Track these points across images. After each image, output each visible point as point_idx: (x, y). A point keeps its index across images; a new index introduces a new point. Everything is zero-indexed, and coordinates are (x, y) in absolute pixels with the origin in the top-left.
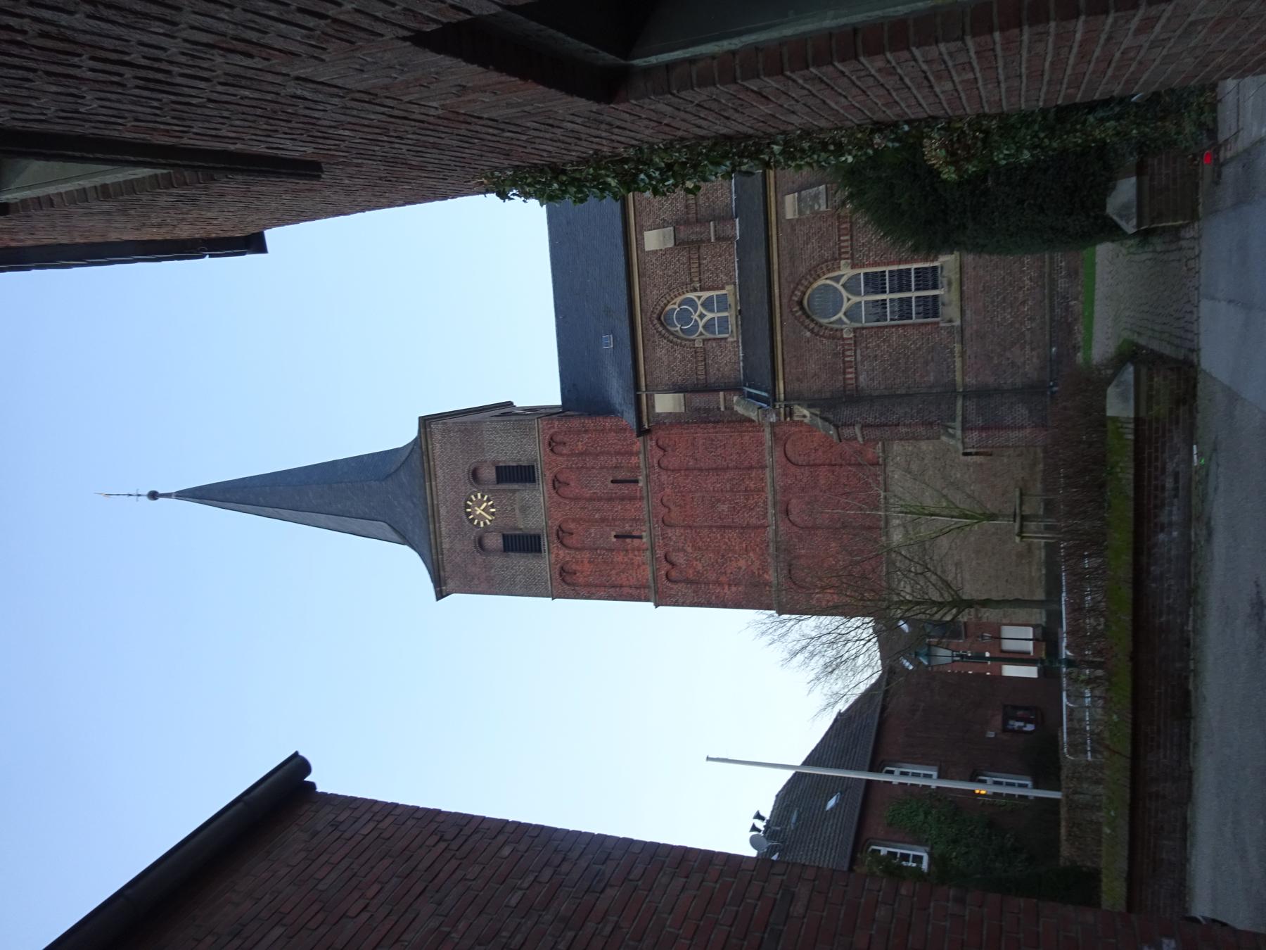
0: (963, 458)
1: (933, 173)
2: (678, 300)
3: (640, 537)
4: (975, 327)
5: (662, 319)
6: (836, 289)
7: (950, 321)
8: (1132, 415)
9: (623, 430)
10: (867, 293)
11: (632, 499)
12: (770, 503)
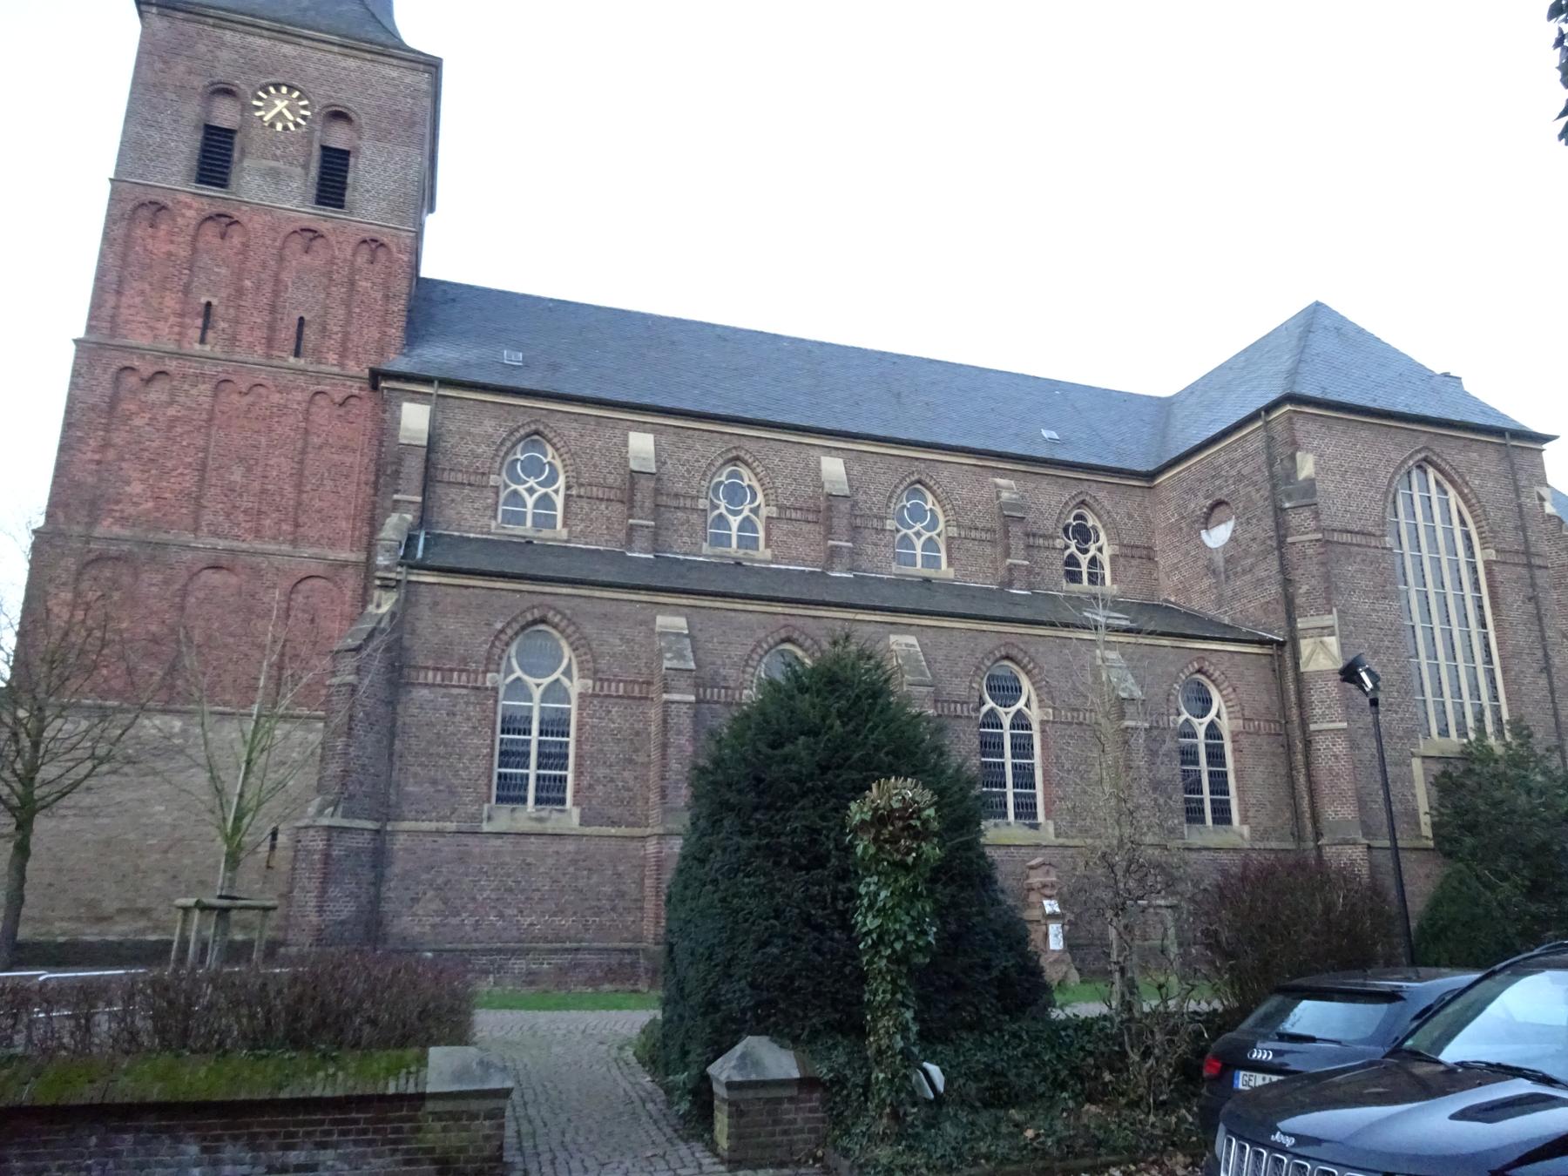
1: (860, 789)
2: (558, 463)
3: (202, 341)
4: (477, 850)
5: (535, 437)
6: (554, 670)
7: (489, 818)
8: (429, 1089)
9: (381, 352)
10: (542, 710)
11: (270, 342)
12: (235, 544)
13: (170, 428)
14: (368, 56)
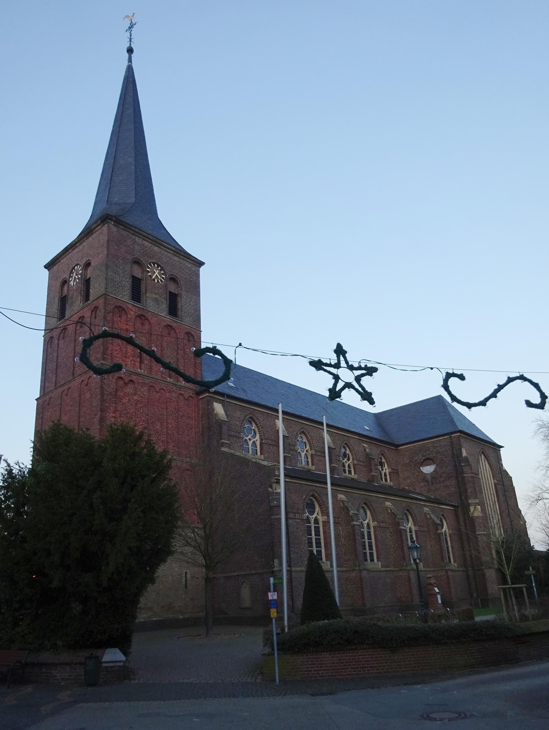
0: (185, 572)
13: (136, 404)
14: (182, 257)
